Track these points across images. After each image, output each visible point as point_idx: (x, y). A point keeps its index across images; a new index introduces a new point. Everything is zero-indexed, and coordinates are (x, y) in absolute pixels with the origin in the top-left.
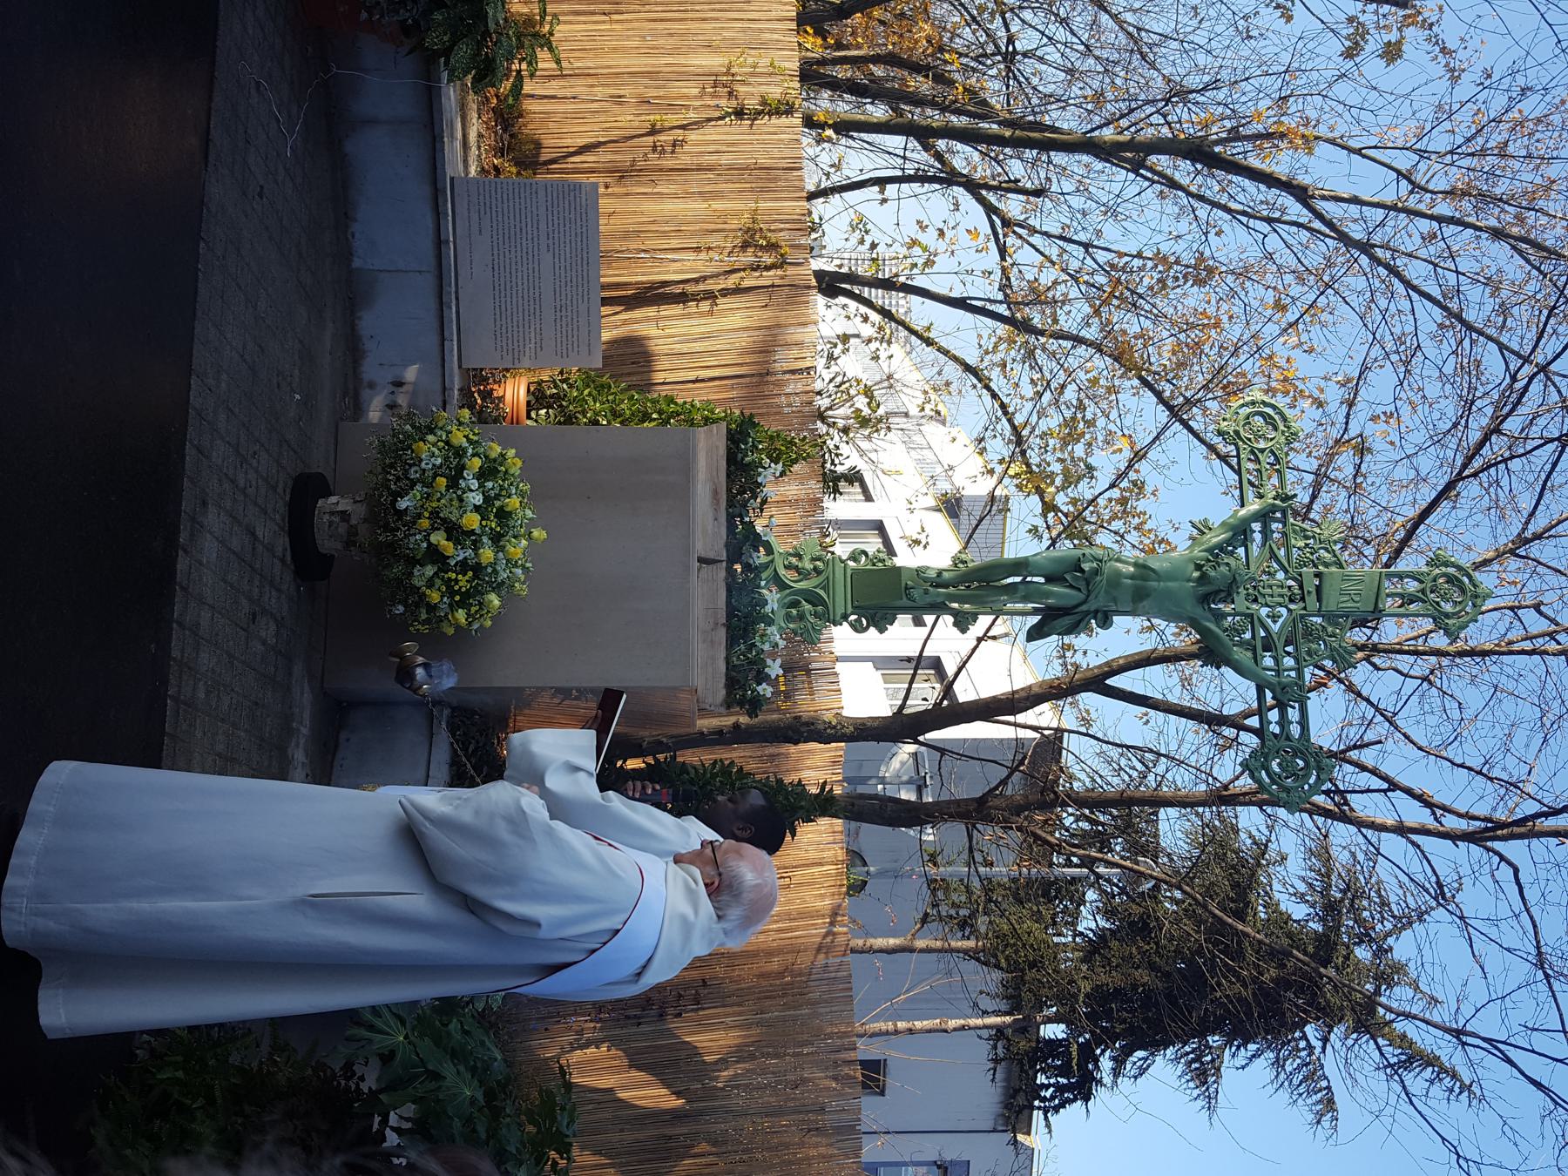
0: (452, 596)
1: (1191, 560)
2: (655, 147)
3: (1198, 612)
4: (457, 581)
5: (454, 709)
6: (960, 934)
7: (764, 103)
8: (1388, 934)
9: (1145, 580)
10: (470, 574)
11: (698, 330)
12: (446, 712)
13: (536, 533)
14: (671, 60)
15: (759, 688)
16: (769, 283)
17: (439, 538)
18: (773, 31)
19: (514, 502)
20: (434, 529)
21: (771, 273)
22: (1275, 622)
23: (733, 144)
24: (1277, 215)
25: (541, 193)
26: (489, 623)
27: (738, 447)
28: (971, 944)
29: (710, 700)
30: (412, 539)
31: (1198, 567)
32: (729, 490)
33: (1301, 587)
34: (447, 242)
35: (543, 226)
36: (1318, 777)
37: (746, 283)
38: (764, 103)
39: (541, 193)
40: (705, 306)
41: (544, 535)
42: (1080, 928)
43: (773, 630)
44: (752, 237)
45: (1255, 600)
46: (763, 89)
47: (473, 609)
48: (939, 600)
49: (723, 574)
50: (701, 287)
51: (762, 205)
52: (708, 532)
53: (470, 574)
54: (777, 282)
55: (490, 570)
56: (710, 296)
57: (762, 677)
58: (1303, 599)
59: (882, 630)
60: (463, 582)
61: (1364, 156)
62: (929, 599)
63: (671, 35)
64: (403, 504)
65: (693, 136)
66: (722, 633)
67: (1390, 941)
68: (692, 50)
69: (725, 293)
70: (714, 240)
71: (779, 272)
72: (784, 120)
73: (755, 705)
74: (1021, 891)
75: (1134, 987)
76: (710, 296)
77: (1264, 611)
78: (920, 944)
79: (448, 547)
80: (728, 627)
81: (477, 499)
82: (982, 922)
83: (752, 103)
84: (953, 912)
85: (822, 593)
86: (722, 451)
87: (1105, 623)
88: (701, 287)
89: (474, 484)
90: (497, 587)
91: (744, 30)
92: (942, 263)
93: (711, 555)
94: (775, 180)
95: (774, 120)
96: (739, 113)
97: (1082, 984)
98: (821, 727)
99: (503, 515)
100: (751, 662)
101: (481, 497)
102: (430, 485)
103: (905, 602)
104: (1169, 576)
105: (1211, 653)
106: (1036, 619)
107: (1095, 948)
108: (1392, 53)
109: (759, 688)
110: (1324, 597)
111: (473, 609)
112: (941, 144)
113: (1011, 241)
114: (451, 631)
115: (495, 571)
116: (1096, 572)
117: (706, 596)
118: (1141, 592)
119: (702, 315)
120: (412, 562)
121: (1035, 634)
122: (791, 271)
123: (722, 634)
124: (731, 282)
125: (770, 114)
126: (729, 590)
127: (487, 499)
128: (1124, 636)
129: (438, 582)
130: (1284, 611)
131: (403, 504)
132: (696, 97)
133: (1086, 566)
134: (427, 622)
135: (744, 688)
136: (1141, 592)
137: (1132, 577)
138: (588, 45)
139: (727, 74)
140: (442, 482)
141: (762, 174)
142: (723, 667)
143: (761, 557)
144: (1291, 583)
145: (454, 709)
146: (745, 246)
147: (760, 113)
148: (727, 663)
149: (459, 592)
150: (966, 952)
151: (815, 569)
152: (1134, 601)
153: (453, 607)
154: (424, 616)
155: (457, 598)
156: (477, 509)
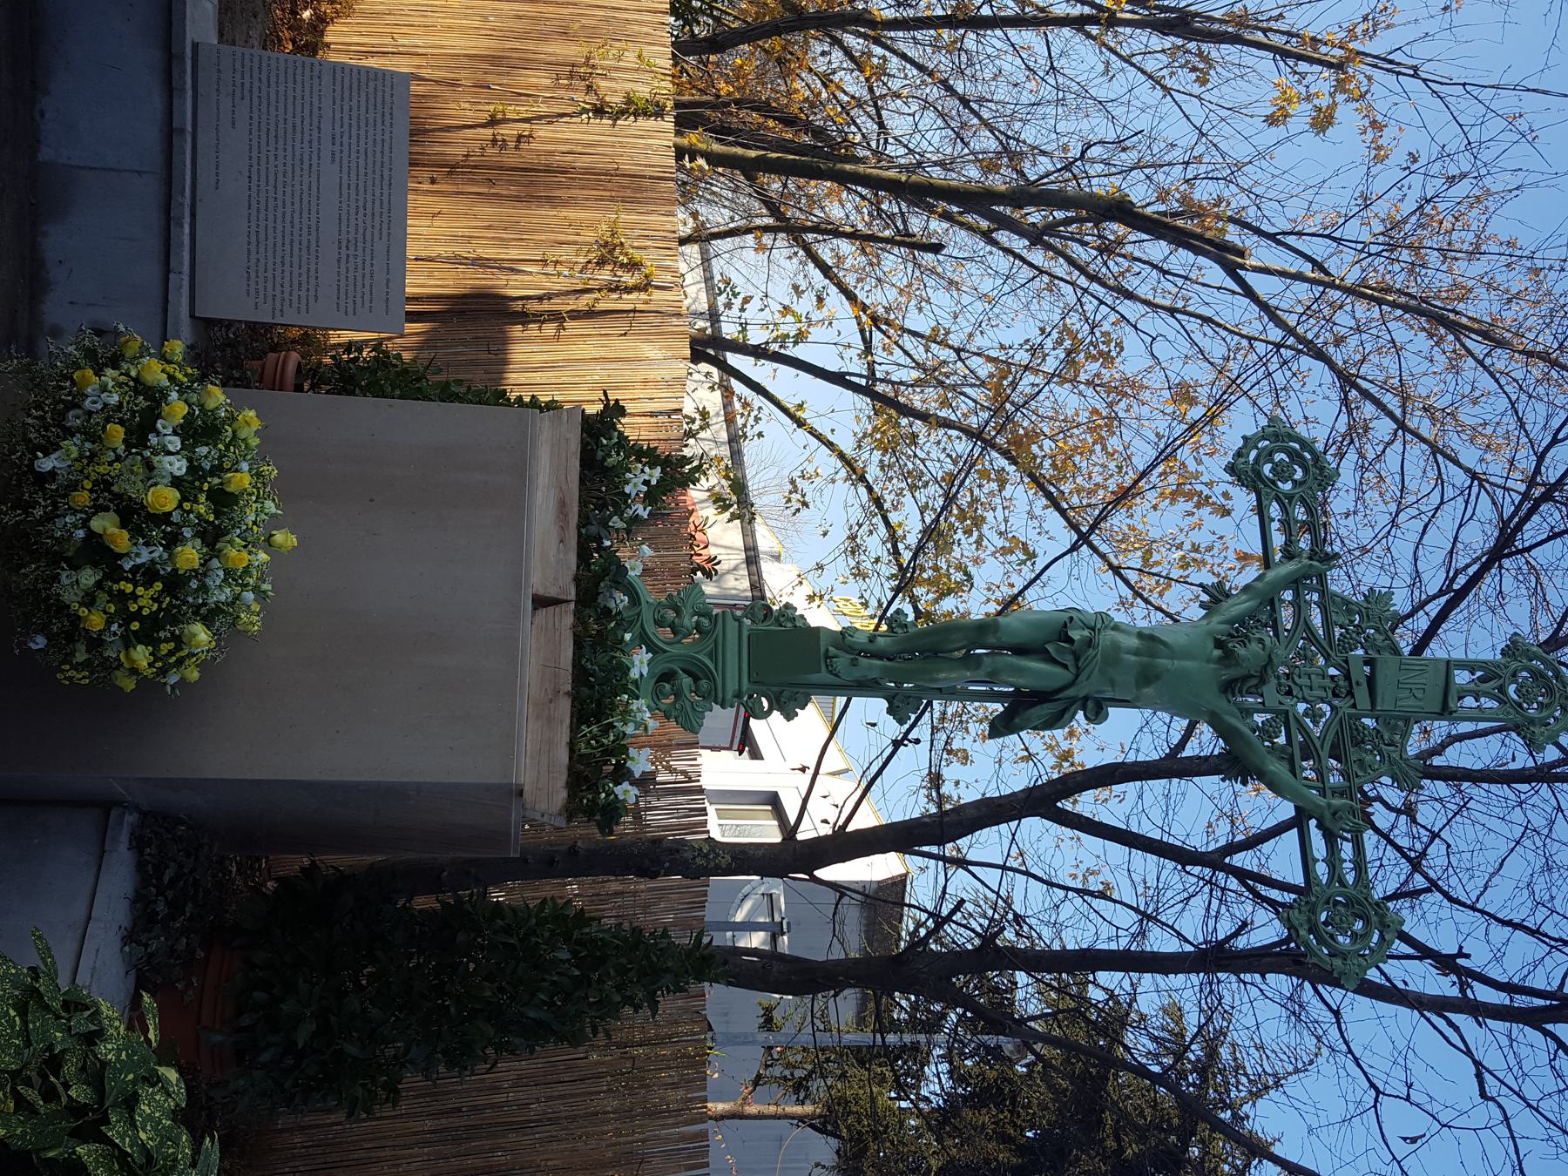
0: (126, 624)
1: (1210, 633)
2: (494, 141)
3: (1220, 704)
4: (134, 597)
5: (144, 815)
6: (794, 1098)
7: (629, 101)
8: (1244, 1102)
9: (1153, 655)
10: (158, 586)
11: (539, 357)
12: (131, 818)
13: (279, 537)
14: (517, 45)
15: (618, 790)
16: (631, 307)
17: (105, 524)
18: (641, 23)
19: (241, 480)
20: (98, 509)
21: (634, 296)
22: (1316, 723)
23: (591, 145)
24: (1180, 304)
25: (327, 79)
26: (194, 675)
27: (598, 442)
28: (808, 1108)
29: (542, 806)
30: (59, 523)
31: (1219, 644)
32: (583, 503)
33: (1348, 677)
34: (182, 131)
35: (326, 126)
36: (1382, 936)
37: (602, 306)
38: (629, 101)
39: (327, 79)
40: (550, 329)
41: (293, 540)
42: (924, 1092)
43: (640, 705)
44: (611, 252)
45: (1289, 693)
46: (629, 86)
47: (165, 648)
48: (872, 675)
49: (569, 620)
50: (546, 306)
51: (623, 216)
52: (549, 561)
53: (158, 586)
54: (640, 307)
55: (194, 584)
56: (557, 317)
57: (621, 774)
58: (1350, 693)
59: (789, 716)
60: (146, 599)
61: (1279, 243)
62: (857, 674)
63: (519, 17)
64: (46, 464)
65: (542, 131)
66: (565, 706)
67: (1246, 1108)
68: (544, 37)
69: (576, 315)
70: (564, 253)
71: (643, 296)
72: (651, 123)
73: (611, 812)
74: (862, 1056)
75: (987, 1162)
76: (557, 317)
77: (1301, 707)
78: (752, 1109)
79: (121, 540)
80: (575, 697)
81: (179, 466)
82: (816, 1085)
83: (616, 100)
84: (787, 1073)
85: (708, 662)
86: (575, 446)
87: (1097, 714)
88: (546, 306)
89: (175, 443)
90: (209, 617)
91: (607, 19)
92: (816, 333)
93: (553, 592)
94: (640, 189)
95: (641, 122)
96: (599, 111)
97: (933, 1162)
98: (688, 855)
99: (223, 500)
100: (609, 752)
101: (184, 463)
102: (94, 437)
103: (824, 676)
104: (1185, 654)
105: (1234, 764)
106: (998, 708)
107: (944, 1119)
108: (1323, 121)
109: (618, 790)
110: (1379, 691)
111: (165, 648)
112: (810, 237)
113: (877, 337)
114: (129, 684)
115: (204, 588)
116: (1089, 643)
117: (545, 651)
118: (1143, 672)
119: (546, 340)
120: (57, 558)
121: (999, 728)
122: (657, 295)
123: (565, 707)
124: (583, 303)
125: (636, 114)
126: (578, 644)
127: (193, 468)
128: (1124, 733)
129: (103, 597)
130: (1326, 708)
131: (46, 464)
132: (547, 88)
133: (1076, 635)
134: (85, 665)
135: (594, 788)
136: (1143, 672)
137: (1137, 653)
138: (417, 21)
139: (586, 64)
140: (117, 433)
141: (625, 181)
142: (563, 756)
143: (621, 600)
144: (1332, 671)
145: (144, 815)
146: (601, 263)
147: (623, 112)
148: (572, 750)
149: (137, 615)
150: (801, 1119)
151: (698, 626)
152: (1139, 686)
153: (128, 642)
154: (80, 657)
155: (135, 626)
156: (176, 482)
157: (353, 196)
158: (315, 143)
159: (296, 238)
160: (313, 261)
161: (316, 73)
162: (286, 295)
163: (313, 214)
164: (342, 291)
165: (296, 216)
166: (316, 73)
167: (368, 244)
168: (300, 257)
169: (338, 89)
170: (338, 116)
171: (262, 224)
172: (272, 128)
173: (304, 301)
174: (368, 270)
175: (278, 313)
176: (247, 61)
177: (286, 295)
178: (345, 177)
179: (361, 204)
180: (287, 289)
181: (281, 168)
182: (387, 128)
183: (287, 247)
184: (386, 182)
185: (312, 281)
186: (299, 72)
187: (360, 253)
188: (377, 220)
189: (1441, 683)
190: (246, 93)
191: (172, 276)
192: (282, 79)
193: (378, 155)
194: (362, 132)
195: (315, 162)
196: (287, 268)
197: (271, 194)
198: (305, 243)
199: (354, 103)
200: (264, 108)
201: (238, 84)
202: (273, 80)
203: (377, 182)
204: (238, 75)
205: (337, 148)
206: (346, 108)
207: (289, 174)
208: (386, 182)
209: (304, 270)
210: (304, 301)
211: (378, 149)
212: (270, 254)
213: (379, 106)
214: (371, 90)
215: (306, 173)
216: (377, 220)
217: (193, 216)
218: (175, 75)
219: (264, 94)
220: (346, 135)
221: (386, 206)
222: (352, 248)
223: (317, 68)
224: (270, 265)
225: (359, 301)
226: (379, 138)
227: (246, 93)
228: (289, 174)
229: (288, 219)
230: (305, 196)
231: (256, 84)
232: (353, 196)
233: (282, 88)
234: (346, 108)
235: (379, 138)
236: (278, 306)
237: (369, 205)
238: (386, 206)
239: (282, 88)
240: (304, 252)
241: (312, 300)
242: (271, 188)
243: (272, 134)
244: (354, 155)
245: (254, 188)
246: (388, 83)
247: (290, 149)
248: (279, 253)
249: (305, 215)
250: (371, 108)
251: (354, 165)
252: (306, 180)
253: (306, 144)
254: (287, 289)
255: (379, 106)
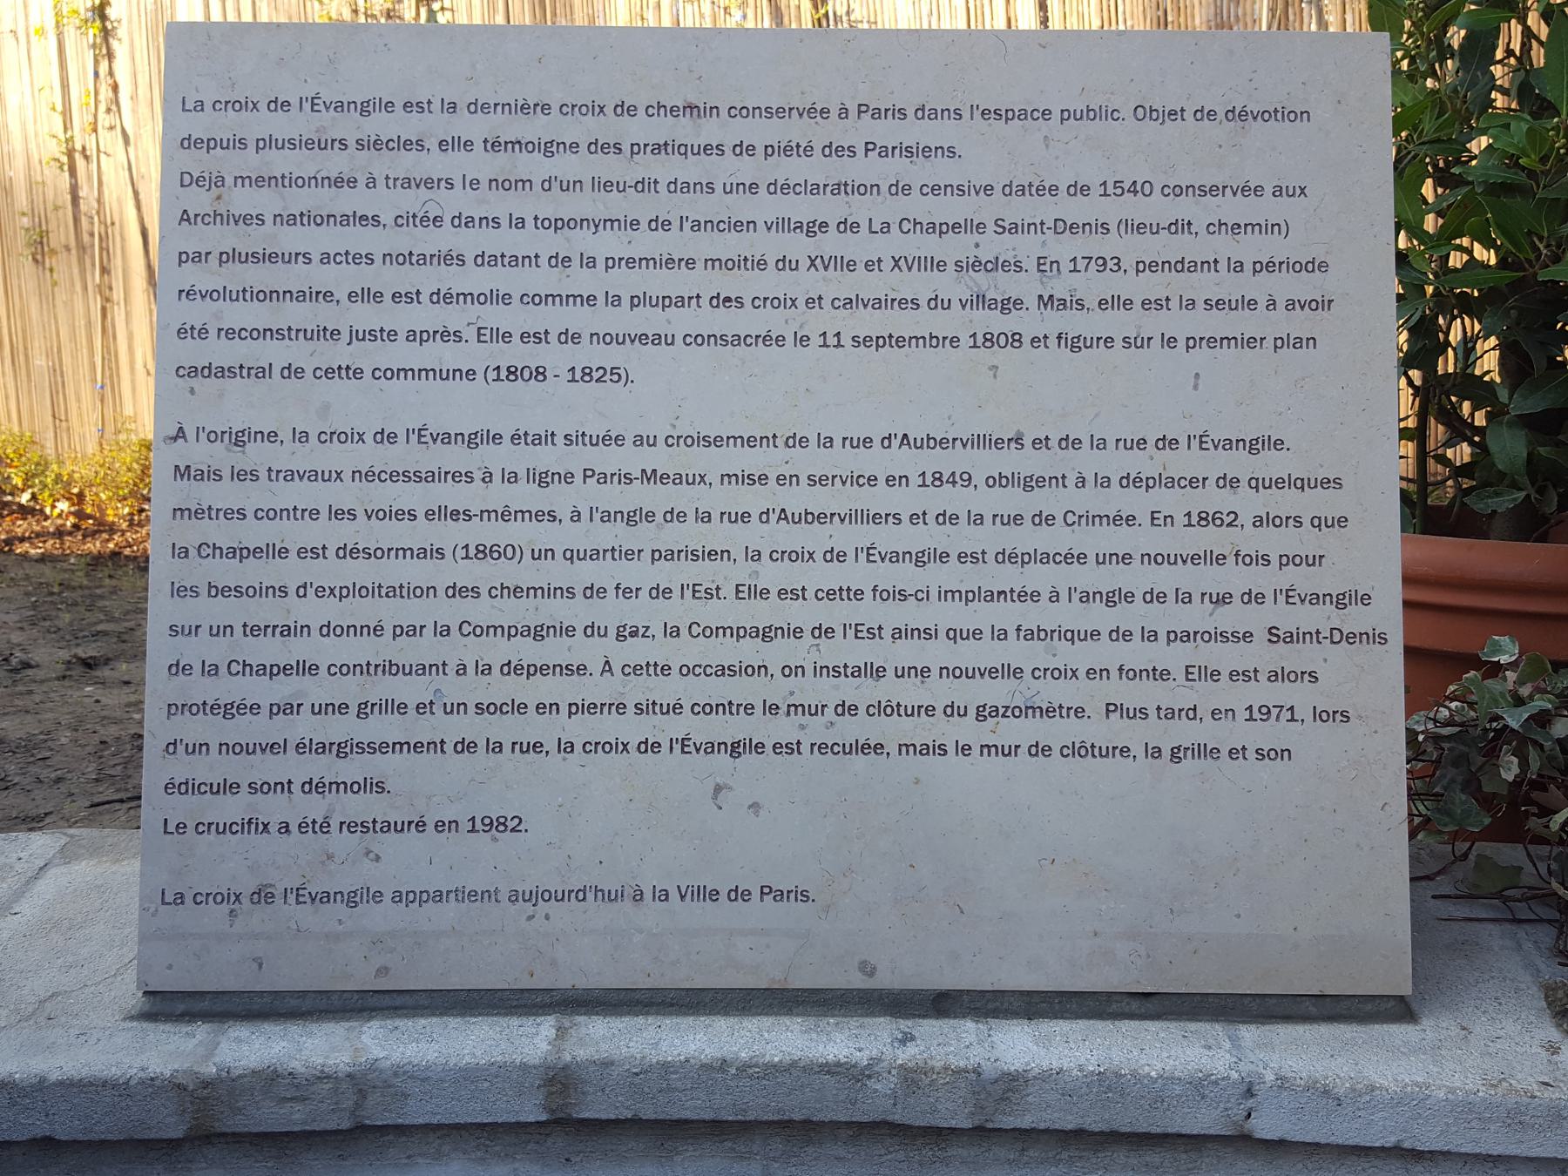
25: (239, 405)
39: (239, 405)
157: (769, 283)
158: (546, 458)
159: (989, 538)
160: (1087, 462)
161: (219, 456)
162: (1266, 579)
163: (876, 461)
164: (1218, 323)
165: (887, 538)
166: (219, 456)
167: (985, 209)
168: (1073, 519)
169: (275, 353)
170: (401, 354)
171: (941, 691)
172: (499, 650)
173: (1286, 502)
174: (1114, 210)
175: (1356, 619)
176: (207, 769)
177: (1266, 579)
178: (681, 321)
179: (799, 246)
180: (1235, 579)
181: (679, 610)
182: (436, 125)
183: (1039, 577)
184: (683, 130)
185: (1184, 462)
186: (222, 533)
187: (1026, 247)
188: (861, 169)
189: (285, 977)
190: (352, 769)
191: (1265, 1126)
192: (266, 611)
193: (565, 166)
194: (470, 242)
195: (631, 459)
196: (1137, 578)
197: (800, 651)
198: (1011, 500)
199: (341, 279)
200: (411, 690)
201: (314, 806)
202: (269, 650)
203: (690, 169)
204: (274, 808)
205: (555, 357)
206: (365, 316)
207: (703, 573)
208: (683, 130)
209: (1137, 502)
210: (1286, 502)
211: (536, 166)
212: (1080, 656)
213: (336, 162)
214: (265, 201)
215: (684, 498)
216: (861, 169)
217: (943, 1004)
218: (295, 1117)
219: (351, 690)
220: (494, 316)
221: (795, 130)
222: (1002, 285)
223: (199, 453)
224: (1137, 654)
225: (1252, 248)
226: (483, 165)
227: (352, 769)
228: (703, 573)
229: (906, 576)
230: (798, 499)
231: (304, 727)
232: (769, 283)
233: (313, 611)
234: (365, 316)
235: (483, 165)
236: (1320, 617)
237: (802, 208)
238: (795, 130)
239: (313, 611)
240: (1047, 500)
241: (1271, 464)
242: (778, 653)
243: (527, 651)
244: (581, 281)
245: (783, 729)
246: (225, 125)
247: (586, 573)
248: (1069, 615)
249: (879, 499)
250: (346, 201)
251: (627, 282)
252: (718, 498)
253: (561, 498)
254: (1235, 579)
255: (336, 162)
